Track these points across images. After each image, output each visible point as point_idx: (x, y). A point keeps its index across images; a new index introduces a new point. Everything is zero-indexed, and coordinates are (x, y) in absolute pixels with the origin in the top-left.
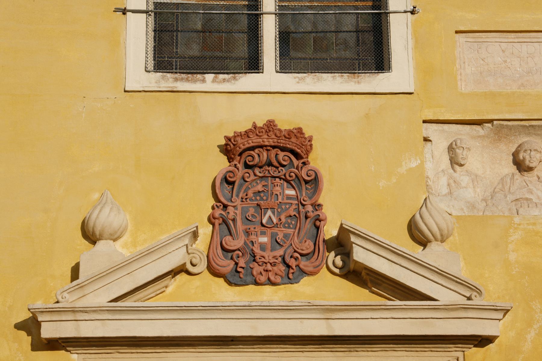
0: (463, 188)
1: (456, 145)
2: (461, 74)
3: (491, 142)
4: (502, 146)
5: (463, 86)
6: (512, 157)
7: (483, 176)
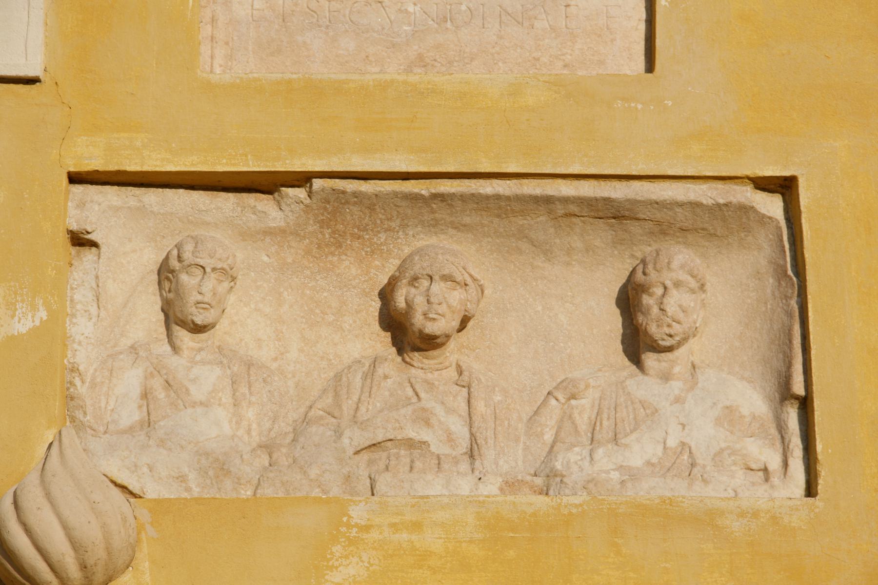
0: (194, 405)
1: (180, 258)
2: (213, 20)
3: (308, 252)
4: (348, 266)
5: (218, 61)
6: (377, 304)
7: (275, 365)
